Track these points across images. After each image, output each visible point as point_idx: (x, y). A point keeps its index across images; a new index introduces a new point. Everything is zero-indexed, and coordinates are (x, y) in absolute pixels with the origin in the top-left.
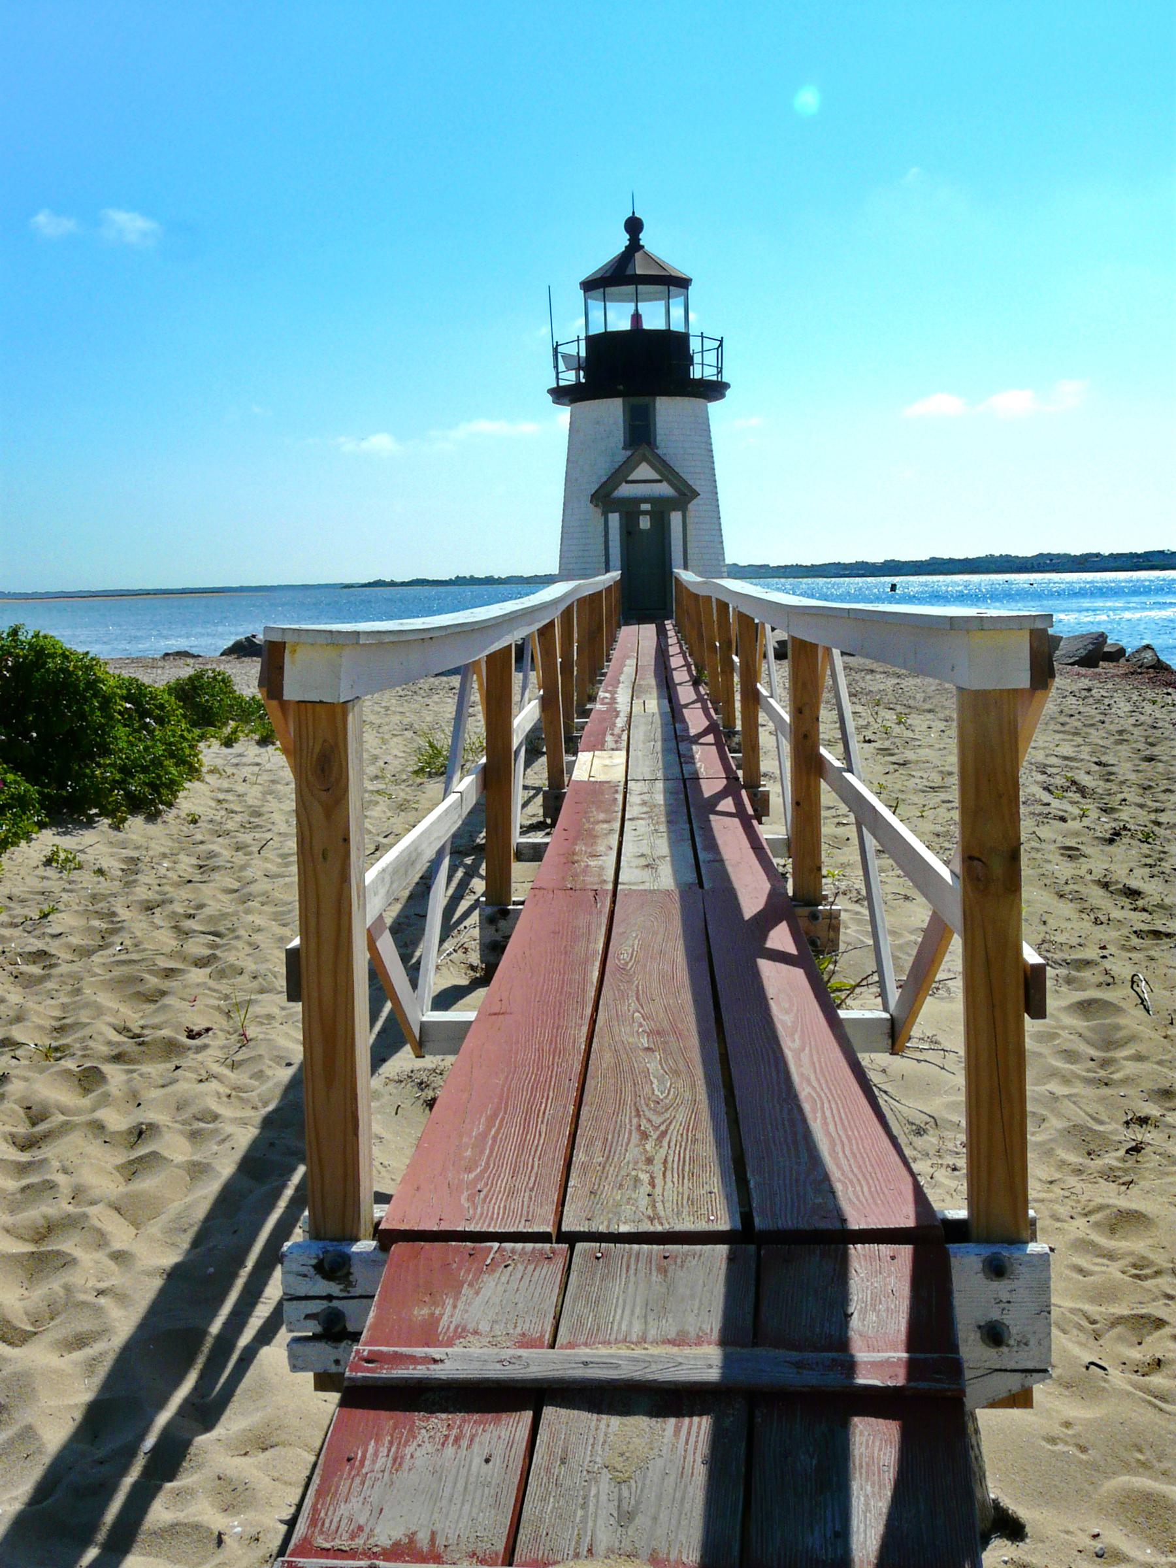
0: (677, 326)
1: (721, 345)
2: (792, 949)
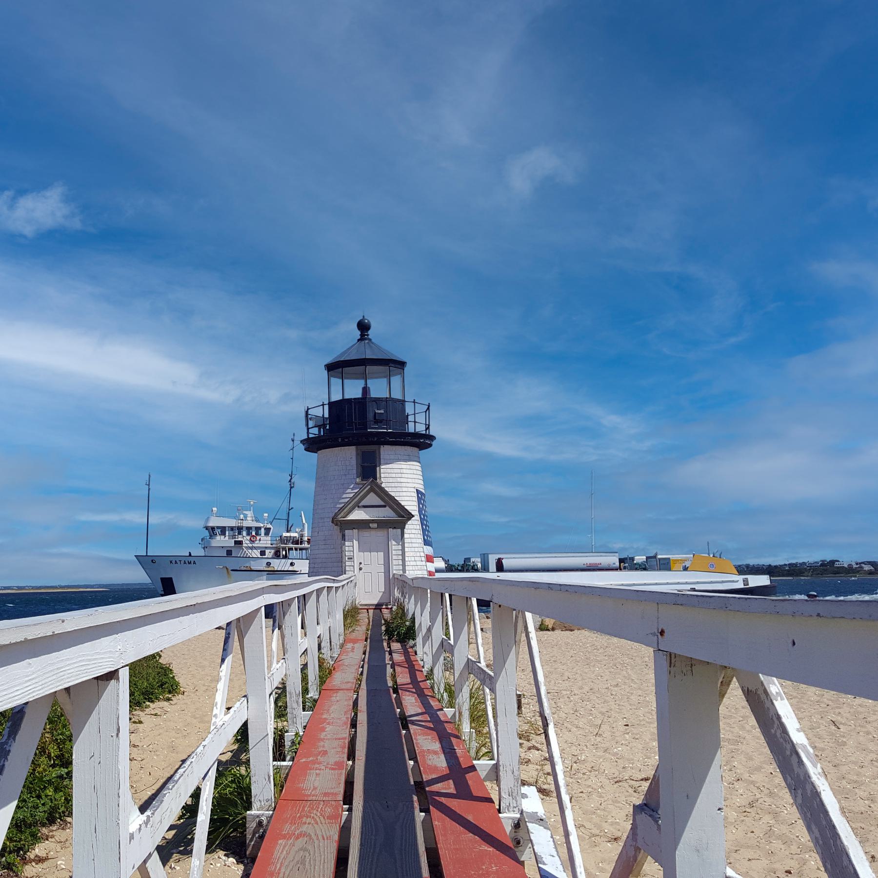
0: (397, 394)
1: (428, 408)
2: (452, 738)
